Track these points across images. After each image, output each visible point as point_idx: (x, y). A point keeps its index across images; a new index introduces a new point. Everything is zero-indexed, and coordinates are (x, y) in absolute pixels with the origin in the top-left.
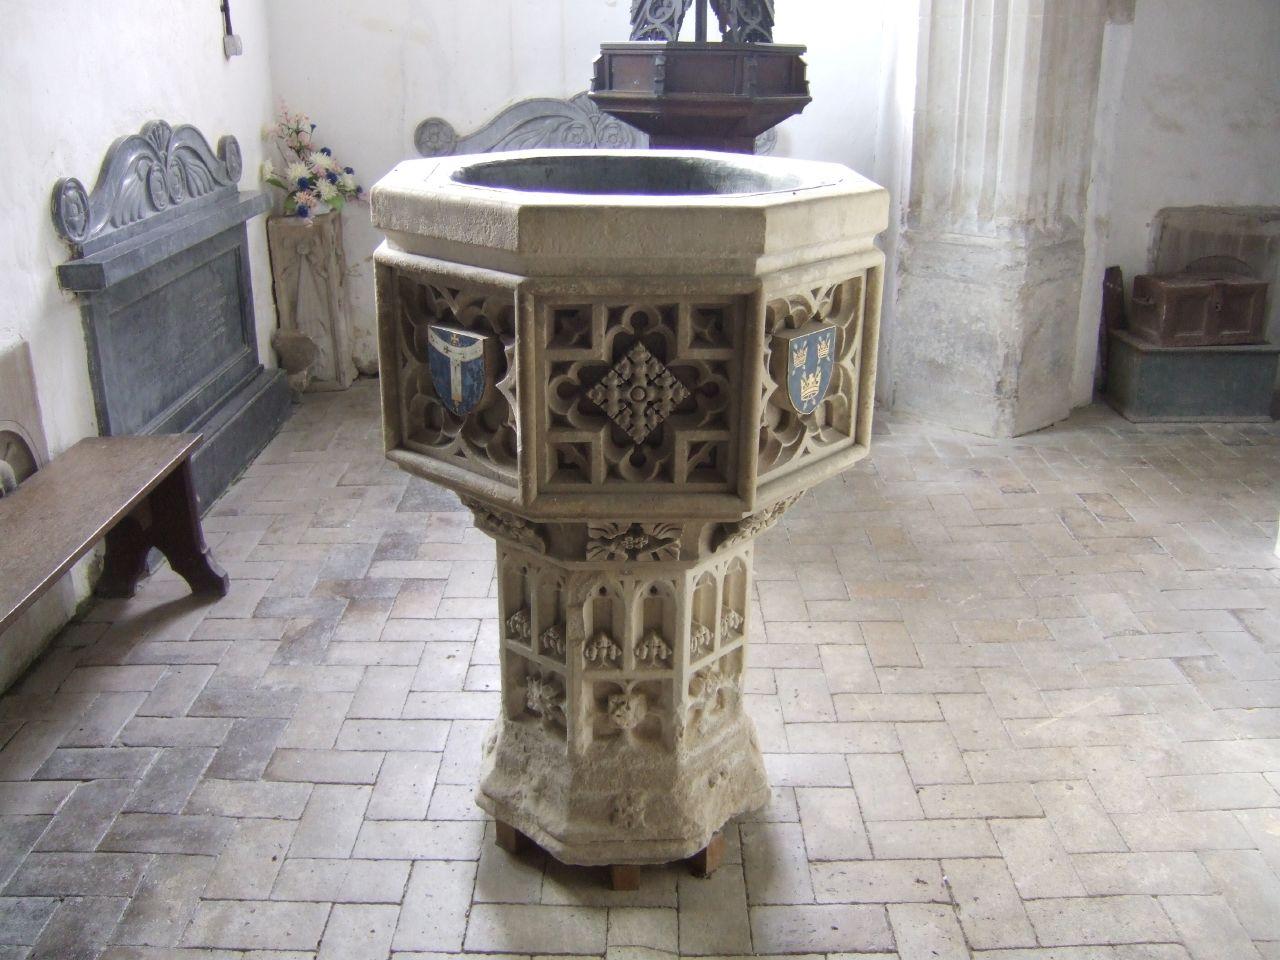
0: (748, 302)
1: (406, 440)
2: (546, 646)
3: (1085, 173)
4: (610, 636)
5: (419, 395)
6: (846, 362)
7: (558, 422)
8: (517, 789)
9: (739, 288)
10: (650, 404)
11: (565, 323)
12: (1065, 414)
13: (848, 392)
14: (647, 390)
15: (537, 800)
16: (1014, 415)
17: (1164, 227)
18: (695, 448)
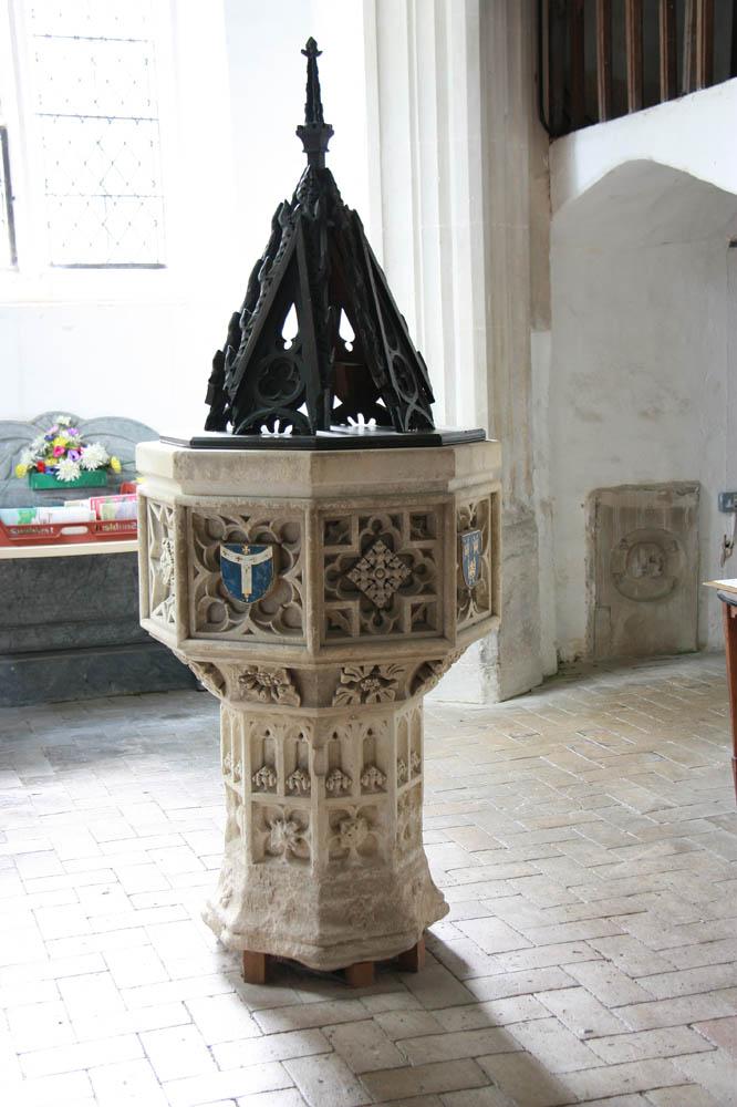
0: (445, 508)
1: (193, 633)
2: (291, 787)
3: (529, 460)
4: (340, 769)
5: (207, 597)
6: (485, 556)
7: (329, 597)
8: (267, 918)
9: (441, 499)
10: (387, 581)
11: (331, 530)
12: (540, 681)
13: (486, 578)
14: (380, 572)
15: (288, 921)
16: (499, 681)
17: (597, 506)
18: (415, 609)
